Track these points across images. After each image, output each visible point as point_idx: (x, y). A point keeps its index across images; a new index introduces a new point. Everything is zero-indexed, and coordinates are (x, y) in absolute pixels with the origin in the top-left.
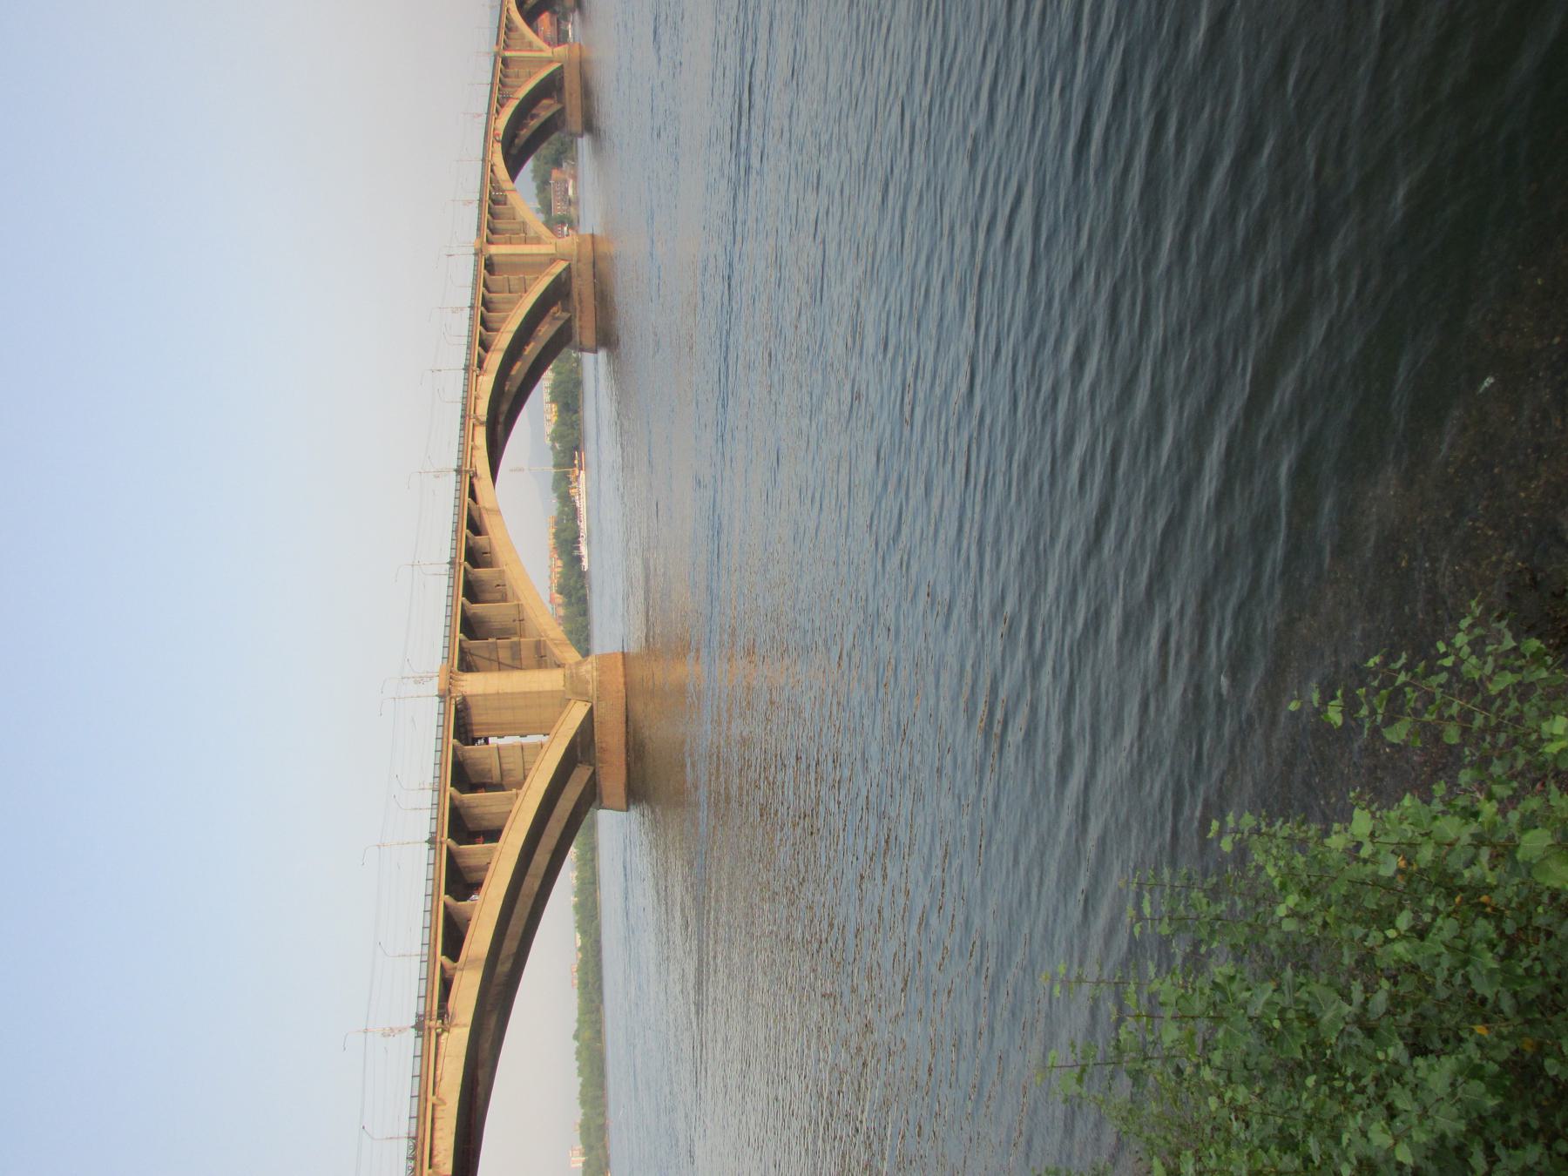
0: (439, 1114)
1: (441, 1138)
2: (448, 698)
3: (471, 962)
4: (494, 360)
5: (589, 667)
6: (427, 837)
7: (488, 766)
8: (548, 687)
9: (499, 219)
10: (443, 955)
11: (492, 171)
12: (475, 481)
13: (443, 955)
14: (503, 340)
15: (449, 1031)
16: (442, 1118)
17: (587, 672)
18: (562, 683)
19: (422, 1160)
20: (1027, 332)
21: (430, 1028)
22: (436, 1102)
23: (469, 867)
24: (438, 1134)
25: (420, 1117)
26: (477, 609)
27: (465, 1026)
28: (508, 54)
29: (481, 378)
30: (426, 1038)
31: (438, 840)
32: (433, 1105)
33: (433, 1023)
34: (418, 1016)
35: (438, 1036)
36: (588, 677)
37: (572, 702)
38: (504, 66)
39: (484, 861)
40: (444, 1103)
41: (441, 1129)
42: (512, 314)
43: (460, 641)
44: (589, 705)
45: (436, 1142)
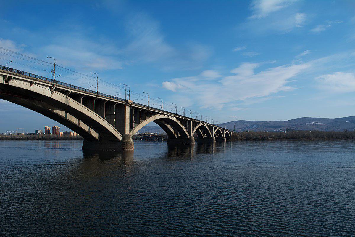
2: (125, 102)
4: (58, 97)
14: (74, 104)
27: (52, 96)
29: (49, 88)
35: (50, 87)
36: (129, 141)
37: (122, 136)
38: (186, 122)
42: (94, 112)
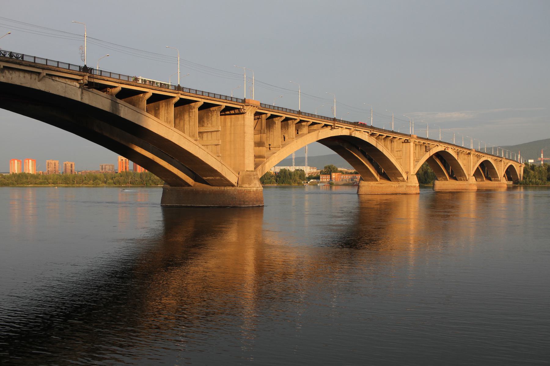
0: (34, 76)
1: (19, 76)
3: (114, 104)
5: (258, 186)
6: (182, 86)
7: (206, 125)
8: (247, 161)
9: (308, 127)
10: (204, 102)
11: (326, 126)
12: (329, 128)
13: (204, 102)
15: (79, 88)
16: (31, 78)
17: (256, 184)
18: (248, 170)
19: (207, 99)
20: (202, 318)
21: (83, 76)
22: (42, 76)
23: (159, 109)
24: (22, 75)
25: (34, 65)
26: (278, 122)
27: (82, 99)
28: (472, 155)
29: (367, 134)
30: (174, 91)
31: (180, 92)
32: (39, 73)
33: (87, 78)
34: (92, 69)
36: (252, 185)
39: (160, 118)
40: (39, 81)
41: (24, 77)
43: (266, 114)
44: (236, 185)
45: (17, 73)
